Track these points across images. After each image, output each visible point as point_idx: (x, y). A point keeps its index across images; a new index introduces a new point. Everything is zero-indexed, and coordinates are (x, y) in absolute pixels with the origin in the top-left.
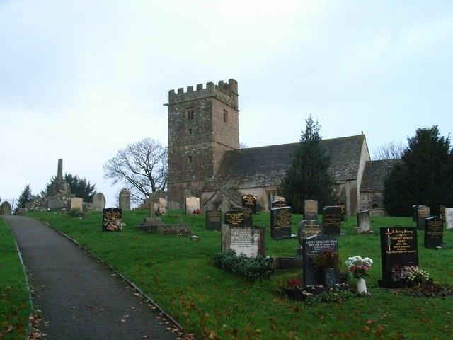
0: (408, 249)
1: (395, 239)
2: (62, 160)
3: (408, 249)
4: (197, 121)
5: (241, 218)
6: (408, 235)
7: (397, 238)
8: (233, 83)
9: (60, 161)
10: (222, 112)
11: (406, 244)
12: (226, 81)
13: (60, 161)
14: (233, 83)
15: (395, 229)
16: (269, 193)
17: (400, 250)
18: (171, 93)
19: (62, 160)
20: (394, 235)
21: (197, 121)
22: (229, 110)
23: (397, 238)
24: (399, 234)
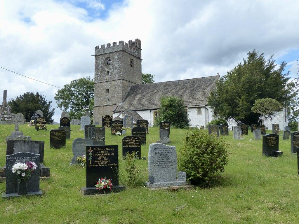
0: (108, 163)
1: (96, 155)
2: (6, 91)
3: (108, 163)
4: (113, 66)
5: (62, 135)
6: (109, 152)
7: (98, 155)
8: (138, 42)
9: (5, 92)
10: (129, 61)
11: (107, 159)
12: (133, 40)
13: (5, 92)
14: (138, 42)
15: (96, 147)
16: (156, 113)
17: (101, 164)
18: (97, 48)
19: (6, 91)
20: (95, 152)
21: (113, 66)
22: (135, 60)
23: (98, 155)
24: (101, 151)
